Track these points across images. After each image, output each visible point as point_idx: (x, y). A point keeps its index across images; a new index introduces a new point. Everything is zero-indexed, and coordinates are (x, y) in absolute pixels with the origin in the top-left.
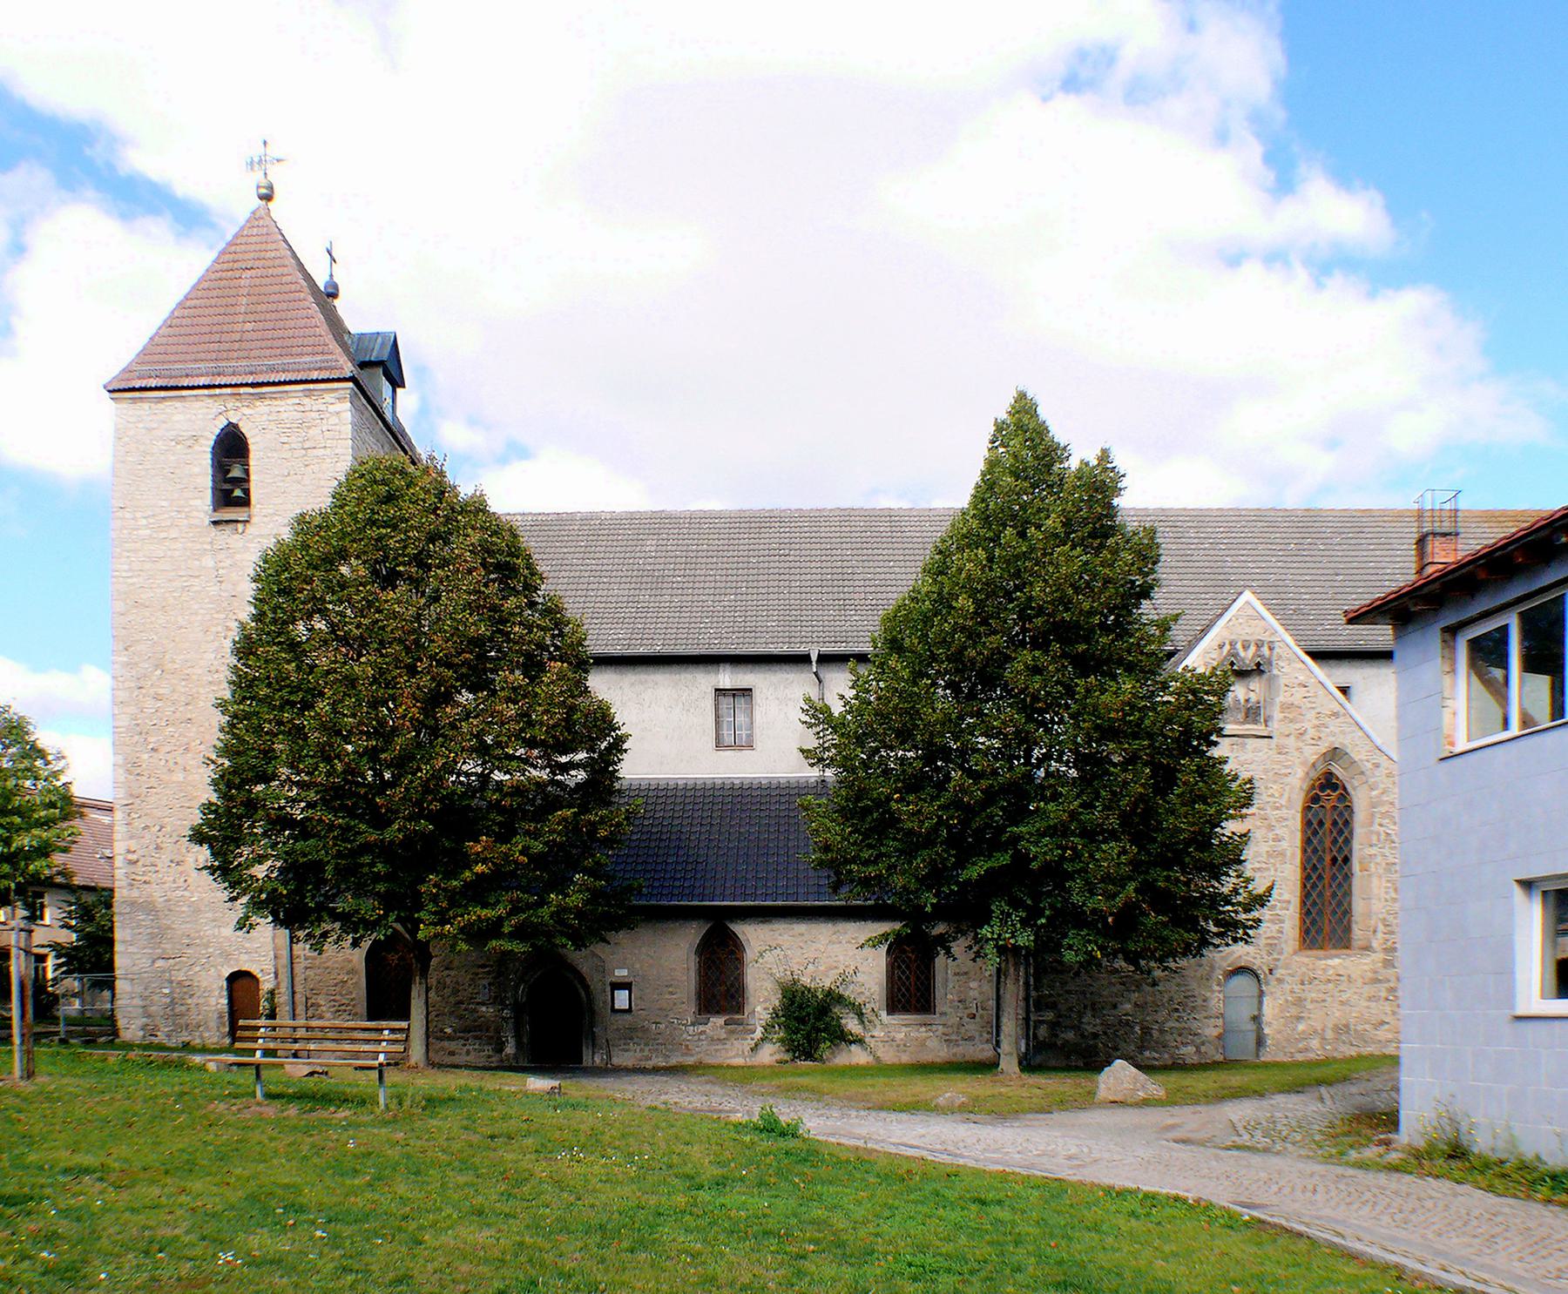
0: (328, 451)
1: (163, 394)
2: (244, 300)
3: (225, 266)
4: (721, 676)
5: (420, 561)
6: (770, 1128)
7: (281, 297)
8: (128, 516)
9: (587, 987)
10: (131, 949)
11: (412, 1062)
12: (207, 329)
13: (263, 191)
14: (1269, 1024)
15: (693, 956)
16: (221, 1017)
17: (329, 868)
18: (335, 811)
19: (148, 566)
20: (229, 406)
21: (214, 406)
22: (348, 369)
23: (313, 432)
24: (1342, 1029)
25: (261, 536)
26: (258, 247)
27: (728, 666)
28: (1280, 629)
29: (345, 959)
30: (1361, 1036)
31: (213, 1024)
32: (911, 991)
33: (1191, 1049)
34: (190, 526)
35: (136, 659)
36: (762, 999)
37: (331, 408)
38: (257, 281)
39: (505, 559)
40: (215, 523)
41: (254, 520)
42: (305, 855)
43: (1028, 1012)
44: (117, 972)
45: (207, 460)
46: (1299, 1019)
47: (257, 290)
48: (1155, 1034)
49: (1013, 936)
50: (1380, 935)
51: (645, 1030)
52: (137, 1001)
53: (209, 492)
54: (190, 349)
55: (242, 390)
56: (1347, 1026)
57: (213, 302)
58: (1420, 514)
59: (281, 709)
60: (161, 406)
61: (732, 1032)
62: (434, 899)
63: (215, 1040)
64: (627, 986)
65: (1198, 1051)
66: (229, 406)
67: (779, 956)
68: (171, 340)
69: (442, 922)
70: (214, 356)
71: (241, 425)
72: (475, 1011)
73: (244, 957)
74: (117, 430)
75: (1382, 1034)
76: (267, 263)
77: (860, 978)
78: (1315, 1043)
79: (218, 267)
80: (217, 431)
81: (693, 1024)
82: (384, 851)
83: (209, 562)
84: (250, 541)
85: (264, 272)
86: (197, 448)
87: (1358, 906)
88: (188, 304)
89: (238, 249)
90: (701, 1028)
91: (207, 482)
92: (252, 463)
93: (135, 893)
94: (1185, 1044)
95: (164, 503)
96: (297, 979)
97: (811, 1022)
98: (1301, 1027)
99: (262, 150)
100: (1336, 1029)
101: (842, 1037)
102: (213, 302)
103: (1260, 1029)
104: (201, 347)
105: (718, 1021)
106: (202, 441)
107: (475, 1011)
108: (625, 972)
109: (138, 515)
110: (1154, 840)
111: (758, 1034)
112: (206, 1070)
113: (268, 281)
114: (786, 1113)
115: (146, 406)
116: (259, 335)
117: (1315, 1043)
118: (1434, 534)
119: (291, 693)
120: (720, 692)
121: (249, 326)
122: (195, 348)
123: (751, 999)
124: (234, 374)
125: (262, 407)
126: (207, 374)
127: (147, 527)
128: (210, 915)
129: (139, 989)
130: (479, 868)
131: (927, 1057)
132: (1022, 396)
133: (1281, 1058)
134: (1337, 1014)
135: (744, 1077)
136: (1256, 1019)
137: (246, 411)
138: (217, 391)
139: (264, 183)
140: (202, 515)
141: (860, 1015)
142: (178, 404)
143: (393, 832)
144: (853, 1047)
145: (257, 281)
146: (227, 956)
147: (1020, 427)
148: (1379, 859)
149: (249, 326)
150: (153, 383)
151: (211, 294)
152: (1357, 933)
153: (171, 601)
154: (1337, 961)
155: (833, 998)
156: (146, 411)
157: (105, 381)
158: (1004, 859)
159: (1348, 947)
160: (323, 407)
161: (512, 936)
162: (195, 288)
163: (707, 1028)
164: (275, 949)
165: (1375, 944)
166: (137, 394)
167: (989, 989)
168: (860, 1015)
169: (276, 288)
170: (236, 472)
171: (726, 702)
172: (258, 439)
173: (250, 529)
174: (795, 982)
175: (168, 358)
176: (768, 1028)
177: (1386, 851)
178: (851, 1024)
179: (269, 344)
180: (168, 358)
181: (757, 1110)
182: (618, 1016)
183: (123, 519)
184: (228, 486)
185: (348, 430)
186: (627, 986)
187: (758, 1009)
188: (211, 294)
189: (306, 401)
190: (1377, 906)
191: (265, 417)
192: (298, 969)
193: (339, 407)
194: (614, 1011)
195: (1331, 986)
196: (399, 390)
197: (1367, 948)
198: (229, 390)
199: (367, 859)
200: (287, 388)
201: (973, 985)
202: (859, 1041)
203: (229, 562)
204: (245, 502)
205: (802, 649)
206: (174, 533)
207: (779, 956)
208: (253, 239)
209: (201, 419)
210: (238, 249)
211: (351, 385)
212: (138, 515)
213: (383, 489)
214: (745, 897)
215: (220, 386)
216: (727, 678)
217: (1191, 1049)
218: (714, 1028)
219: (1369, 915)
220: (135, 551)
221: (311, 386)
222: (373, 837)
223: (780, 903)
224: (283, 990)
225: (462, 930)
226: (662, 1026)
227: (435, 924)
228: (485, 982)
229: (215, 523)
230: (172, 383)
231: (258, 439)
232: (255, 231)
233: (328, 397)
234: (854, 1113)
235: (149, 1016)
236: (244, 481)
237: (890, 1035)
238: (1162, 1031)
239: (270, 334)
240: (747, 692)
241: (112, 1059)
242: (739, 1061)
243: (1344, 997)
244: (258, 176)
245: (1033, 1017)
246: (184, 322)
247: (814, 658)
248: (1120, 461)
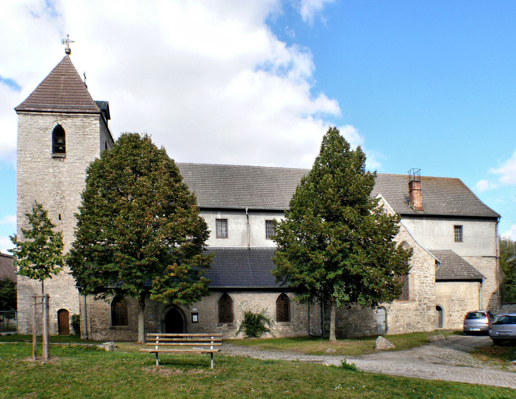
0: (92, 136)
1: (35, 113)
2: (62, 85)
3: (55, 74)
4: (218, 215)
5: (149, 169)
6: (345, 367)
7: (75, 85)
8: (23, 153)
9: (184, 315)
10: (23, 302)
11: (139, 341)
12: (50, 93)
13: (67, 51)
14: (389, 323)
16: (55, 325)
17: (120, 273)
18: (124, 253)
19: (29, 170)
20: (58, 119)
21: (53, 119)
22: (99, 110)
23: (87, 129)
24: (409, 324)
25: (69, 163)
26: (66, 69)
27: (220, 212)
28: (389, 206)
29: (103, 305)
30: (413, 326)
32: (283, 314)
33: (368, 331)
34: (45, 158)
35: (25, 202)
36: (239, 319)
37: (93, 122)
38: (67, 79)
39: (172, 170)
40: (54, 157)
41: (67, 157)
42: (111, 269)
43: (322, 321)
44: (18, 310)
45: (51, 136)
46: (397, 321)
47: (66, 82)
48: (358, 327)
49: (343, 297)
50: (417, 296)
51: (203, 328)
52: (25, 320)
53: (51, 147)
54: (45, 99)
55: (63, 114)
56: (410, 324)
57: (52, 84)
58: (410, 177)
59: (102, 217)
60: (35, 117)
61: (230, 329)
62: (156, 285)
63: (53, 333)
64: (196, 314)
65: (370, 332)
66: (58, 119)
67: (244, 304)
68: (38, 96)
69: (159, 293)
70: (53, 102)
71: (62, 125)
72: (148, 323)
73: (63, 304)
74: (19, 124)
75: (419, 326)
76: (70, 74)
77: (268, 311)
78: (401, 329)
79: (53, 73)
80: (54, 127)
81: (218, 326)
82: (140, 268)
83: (51, 170)
84: (66, 164)
85: (69, 77)
86: (47, 132)
87: (411, 288)
88: (43, 84)
89: (60, 68)
90: (220, 327)
91: (50, 143)
92: (66, 138)
93: (25, 282)
94: (366, 330)
95: (36, 150)
96: (87, 312)
97: (254, 324)
98: (398, 324)
99: (67, 38)
100: (407, 324)
101: (264, 330)
102: (52, 84)
103: (386, 325)
104: (48, 99)
105: (225, 325)
106: (49, 130)
107: (148, 323)
108: (196, 309)
109: (26, 153)
111: (238, 329)
112: (105, 351)
113: (71, 79)
114: (349, 362)
115: (29, 117)
116: (68, 97)
117: (401, 329)
118: (415, 181)
119: (105, 211)
120: (217, 220)
121: (64, 93)
122: (46, 99)
123: (236, 318)
124: (60, 108)
125: (69, 120)
126: (51, 108)
127: (29, 157)
128: (51, 290)
129: (26, 316)
130: (172, 274)
131: (288, 335)
133: (393, 334)
134: (407, 320)
135: (236, 343)
136: (386, 322)
138: (54, 114)
139: (67, 48)
140: (49, 154)
141: (269, 323)
142: (41, 117)
143: (144, 262)
144: (267, 333)
145: (67, 79)
146: (57, 304)
147: (333, 138)
148: (416, 274)
149: (64, 93)
150: (32, 109)
151: (51, 82)
152: (411, 296)
153: (38, 183)
154: (406, 304)
155: (260, 317)
156: (29, 119)
157: (16, 106)
158: (340, 272)
159: (408, 300)
160: (90, 122)
161: (181, 298)
162: (45, 80)
163: (222, 327)
164: (80, 301)
165: (416, 299)
166: (26, 113)
167: (306, 314)
168: (269, 323)
169: (73, 82)
170: (60, 141)
171: (219, 223)
172: (68, 130)
173: (66, 160)
174: (250, 312)
175: (36, 101)
176: (241, 327)
177: (418, 272)
178: (266, 326)
179: (72, 100)
180: (36, 101)
181: (296, 358)
182: (194, 324)
183: (21, 154)
184: (57, 146)
185: (98, 130)
186: (196, 314)
187: (238, 321)
188: (51, 82)
189: (84, 119)
190: (416, 288)
191: (70, 124)
192: (88, 309)
193: (95, 122)
194: (193, 322)
195: (405, 312)
196: (109, 120)
197: (414, 300)
198: (58, 114)
199: (134, 271)
200: (78, 114)
201: (301, 313)
202: (268, 331)
203: (58, 171)
204: (64, 151)
205: (243, 207)
206: (39, 160)
207: (244, 304)
208: (65, 66)
209: (49, 122)
210: (60, 68)
211: (99, 115)
212: (26, 153)
213: (134, 144)
214: (241, 285)
215: (55, 112)
216: (219, 216)
217: (368, 331)
218: (224, 328)
219: (414, 290)
220: (25, 165)
221: (87, 115)
222: (138, 263)
223: (245, 287)
224: (83, 316)
225: (166, 296)
227: (157, 294)
228: (151, 313)
229: (54, 157)
230: (39, 109)
231: (68, 130)
232: (65, 63)
233: (92, 119)
235: (29, 325)
236: (64, 144)
237: (277, 329)
238: (360, 326)
239: (72, 97)
240: (225, 221)
241: (64, 347)
242: (232, 338)
243: (409, 315)
244: (65, 46)
245: (324, 323)
246: (42, 90)
247: (247, 210)
248: (364, 150)
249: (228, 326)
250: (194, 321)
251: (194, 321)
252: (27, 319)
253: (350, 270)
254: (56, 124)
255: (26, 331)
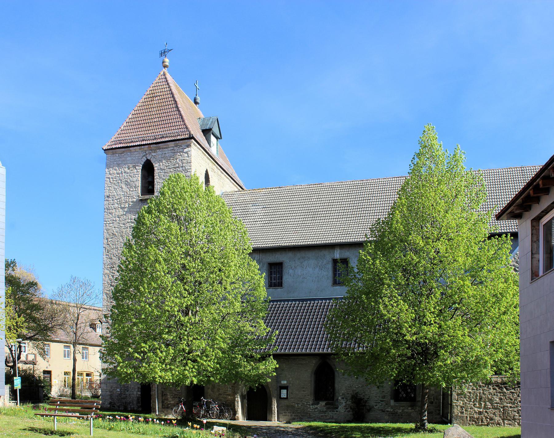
15: (313, 375)
31: (135, 402)
64: (286, 388)
81: (312, 405)
90: (316, 406)
108: (285, 382)
110: (487, 327)
120: (335, 261)
123: (337, 394)
132: (257, 251)
137: (153, 154)
163: (318, 406)
186: (286, 388)
216: (337, 254)
226: (300, 405)
234: (132, 417)
249: (326, 404)
250: (282, 397)
251: (282, 397)
252: (110, 392)
253: (460, 289)
254: (144, 159)
255: (109, 406)
